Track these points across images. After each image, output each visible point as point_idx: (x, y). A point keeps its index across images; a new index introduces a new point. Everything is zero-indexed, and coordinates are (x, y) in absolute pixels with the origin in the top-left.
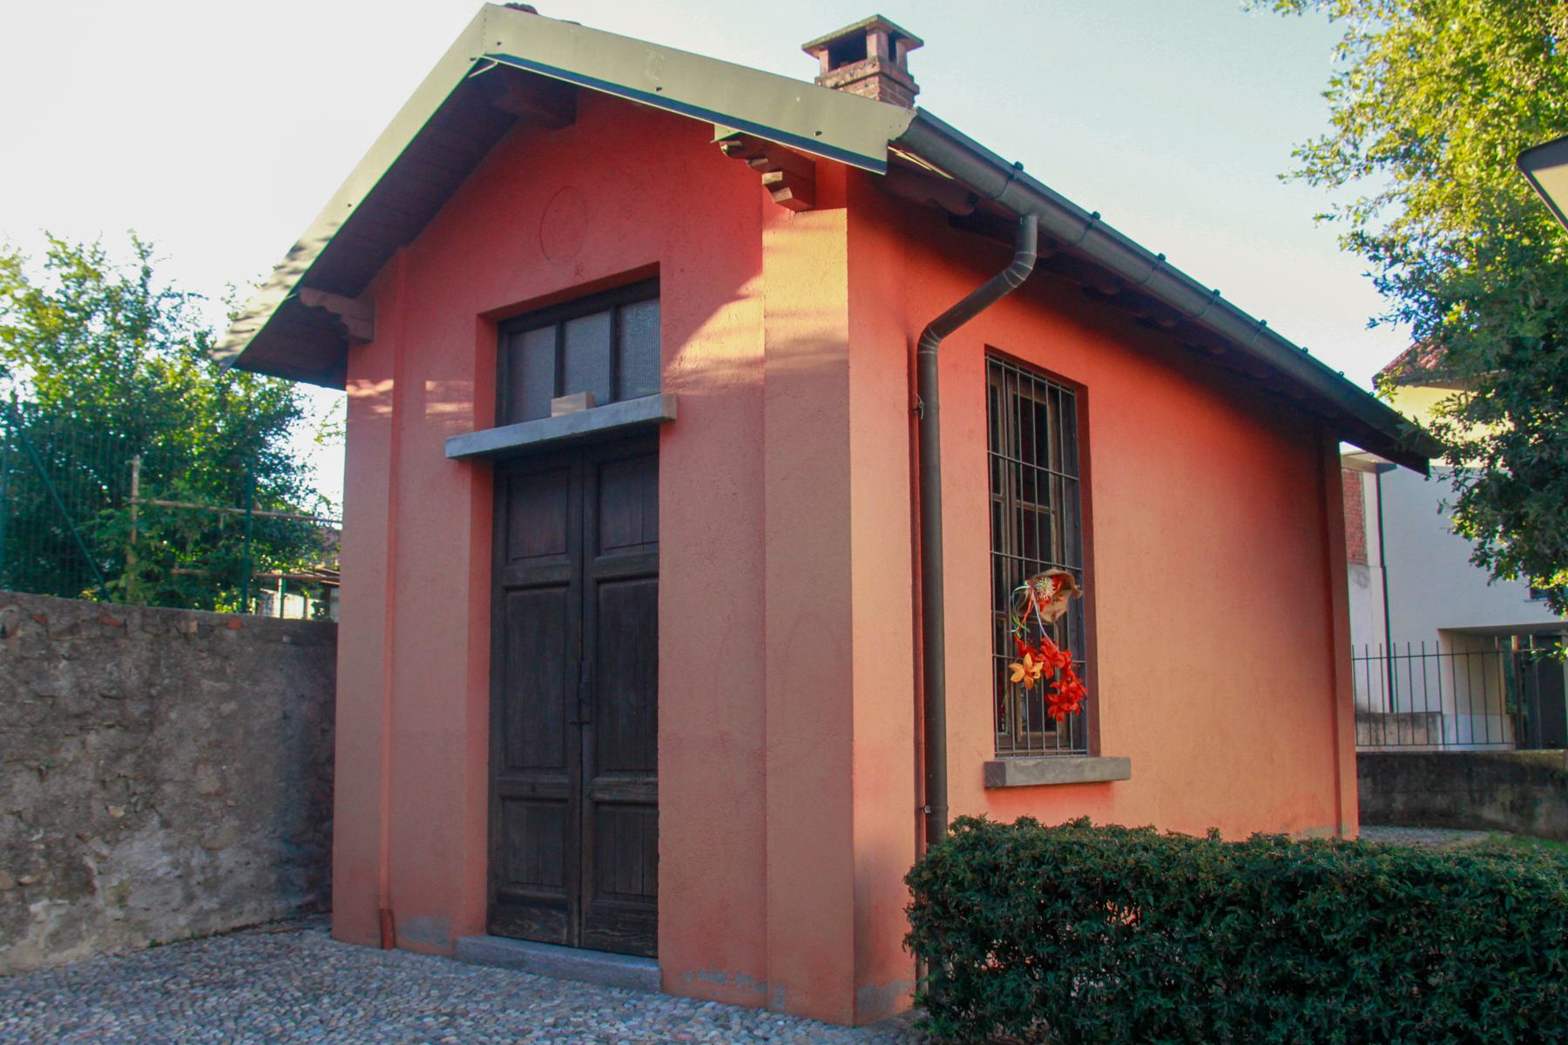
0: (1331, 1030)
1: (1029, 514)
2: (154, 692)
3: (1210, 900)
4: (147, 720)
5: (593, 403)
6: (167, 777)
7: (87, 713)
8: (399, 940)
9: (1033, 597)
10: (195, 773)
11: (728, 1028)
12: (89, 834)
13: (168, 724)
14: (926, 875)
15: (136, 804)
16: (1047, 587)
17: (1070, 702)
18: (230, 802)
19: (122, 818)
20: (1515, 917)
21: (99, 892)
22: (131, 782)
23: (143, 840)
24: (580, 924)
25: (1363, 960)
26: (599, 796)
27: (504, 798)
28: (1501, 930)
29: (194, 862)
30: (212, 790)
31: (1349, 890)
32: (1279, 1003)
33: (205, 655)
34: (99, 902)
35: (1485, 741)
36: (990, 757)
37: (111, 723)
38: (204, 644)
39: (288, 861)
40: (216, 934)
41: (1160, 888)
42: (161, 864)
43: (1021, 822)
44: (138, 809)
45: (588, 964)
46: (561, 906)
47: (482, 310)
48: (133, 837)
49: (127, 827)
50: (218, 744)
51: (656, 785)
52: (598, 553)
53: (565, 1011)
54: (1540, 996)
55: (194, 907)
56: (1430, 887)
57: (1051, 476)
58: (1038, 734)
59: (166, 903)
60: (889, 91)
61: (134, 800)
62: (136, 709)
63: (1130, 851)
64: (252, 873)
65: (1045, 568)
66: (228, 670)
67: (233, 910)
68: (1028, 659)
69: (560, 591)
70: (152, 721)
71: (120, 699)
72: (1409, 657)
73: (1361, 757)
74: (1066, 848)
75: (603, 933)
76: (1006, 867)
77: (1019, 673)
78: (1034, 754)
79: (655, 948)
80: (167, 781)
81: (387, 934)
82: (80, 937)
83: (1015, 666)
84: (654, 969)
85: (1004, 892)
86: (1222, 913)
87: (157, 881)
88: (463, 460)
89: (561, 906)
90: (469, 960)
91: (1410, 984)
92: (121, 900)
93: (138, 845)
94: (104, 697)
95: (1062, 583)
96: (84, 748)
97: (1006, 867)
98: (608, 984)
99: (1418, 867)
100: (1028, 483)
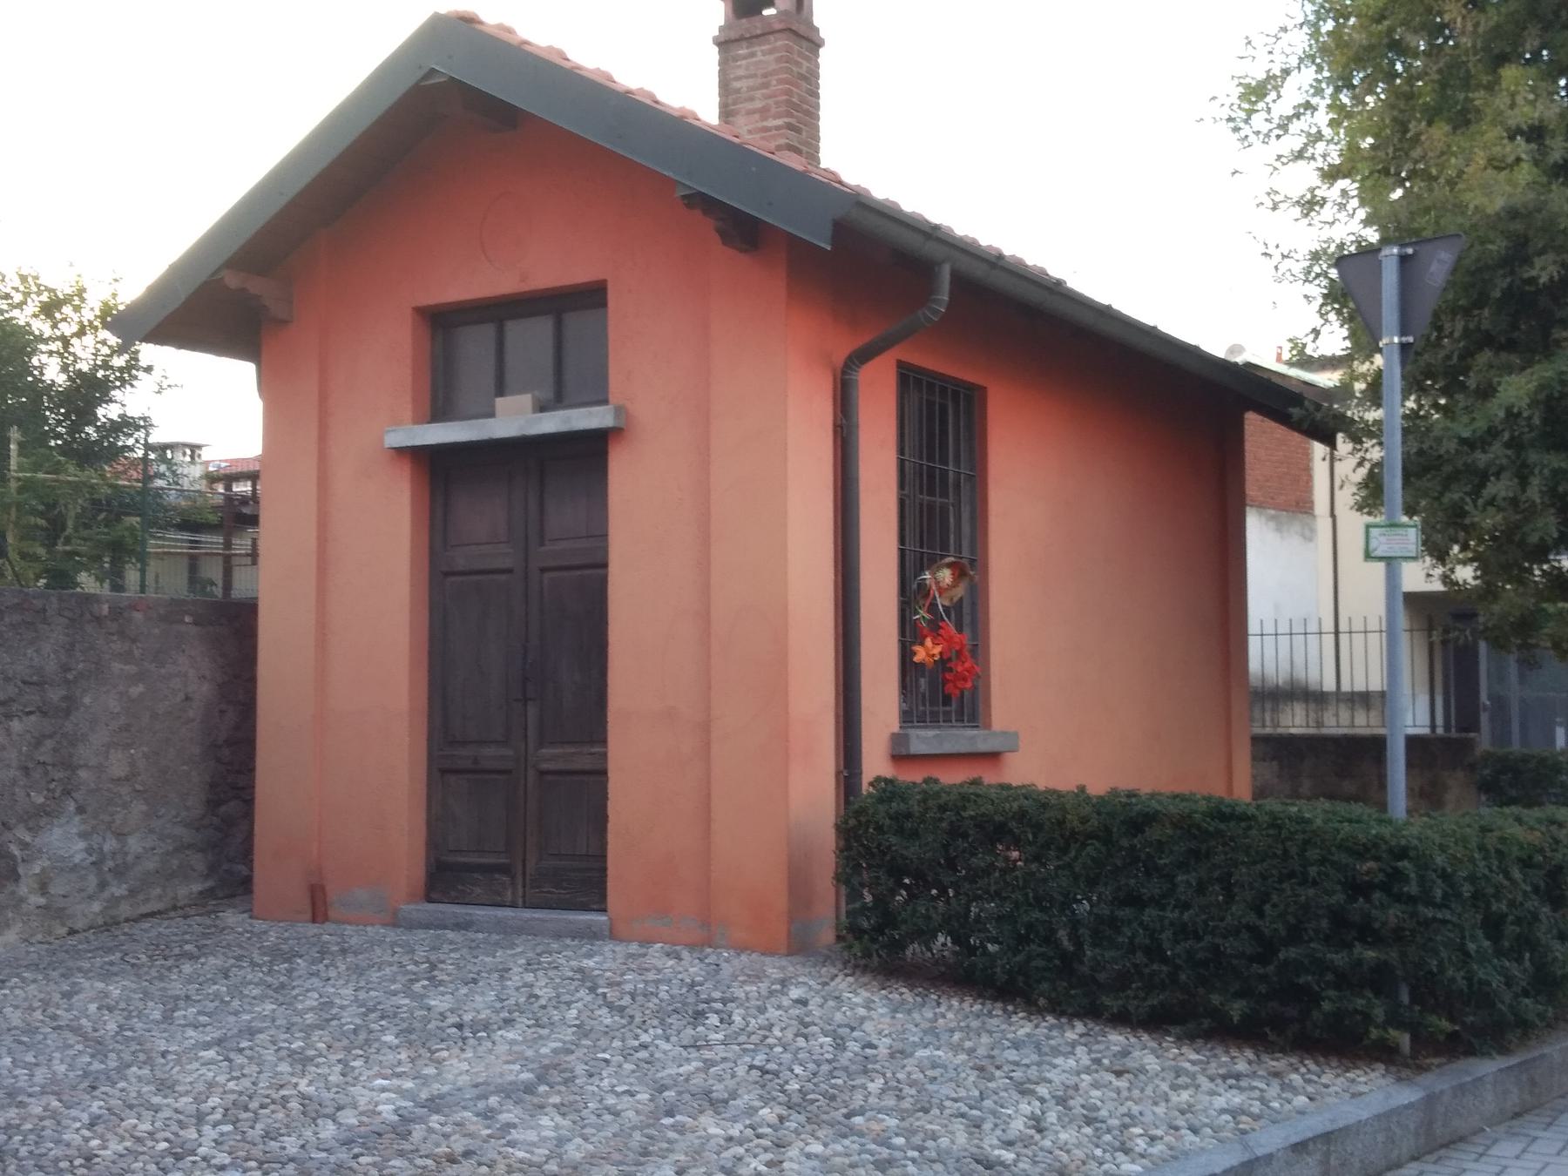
0: (1162, 931)
1: (931, 507)
2: (70, 676)
3: (1073, 833)
4: (64, 705)
5: (542, 407)
6: (82, 762)
7: (12, 700)
8: (331, 914)
9: (934, 587)
10: (107, 758)
11: (681, 959)
12: (13, 821)
13: (82, 709)
14: (852, 822)
15: (53, 791)
16: (946, 576)
17: (965, 679)
18: (138, 787)
19: (43, 805)
20: (1289, 843)
21: (23, 880)
22: (49, 768)
23: (60, 826)
24: (524, 887)
25: (1185, 877)
26: (545, 766)
27: (444, 772)
28: (1279, 852)
29: (106, 848)
30: (123, 774)
31: (1175, 826)
32: (1125, 913)
33: (115, 638)
34: (23, 890)
35: (1380, 724)
36: (896, 728)
37: (32, 709)
38: (113, 627)
39: (189, 846)
40: (127, 920)
41: (1038, 827)
42: (77, 850)
43: (926, 781)
44: (57, 795)
45: (538, 919)
46: (505, 869)
47: (419, 304)
48: (52, 824)
49: (48, 814)
50: (126, 728)
51: (605, 755)
52: (542, 544)
53: (530, 955)
54: (1303, 898)
55: (106, 894)
56: (1232, 824)
57: (951, 473)
58: (936, 709)
59: (83, 890)
60: (796, 47)
61: (52, 786)
62: (55, 695)
63: (1015, 800)
64: (157, 858)
65: (943, 557)
66: (136, 652)
67: (141, 897)
68: (928, 642)
69: (503, 577)
70: (70, 705)
71: (40, 684)
72: (1366, 632)
73: (1256, 740)
74: (964, 797)
75: (548, 892)
76: (917, 814)
77: (920, 655)
78: (933, 728)
79: (603, 897)
80: (81, 766)
81: (318, 907)
82: (8, 926)
83: (917, 648)
84: (603, 918)
85: (915, 834)
86: (1084, 845)
87: (74, 868)
88: (401, 451)
89: (505, 869)
90: (411, 926)
91: (1217, 895)
92: (43, 888)
93: (57, 832)
94: (24, 682)
95: (960, 572)
96: (9, 735)
97: (917, 814)
98: (558, 936)
99: (1224, 809)
100: (931, 477)
